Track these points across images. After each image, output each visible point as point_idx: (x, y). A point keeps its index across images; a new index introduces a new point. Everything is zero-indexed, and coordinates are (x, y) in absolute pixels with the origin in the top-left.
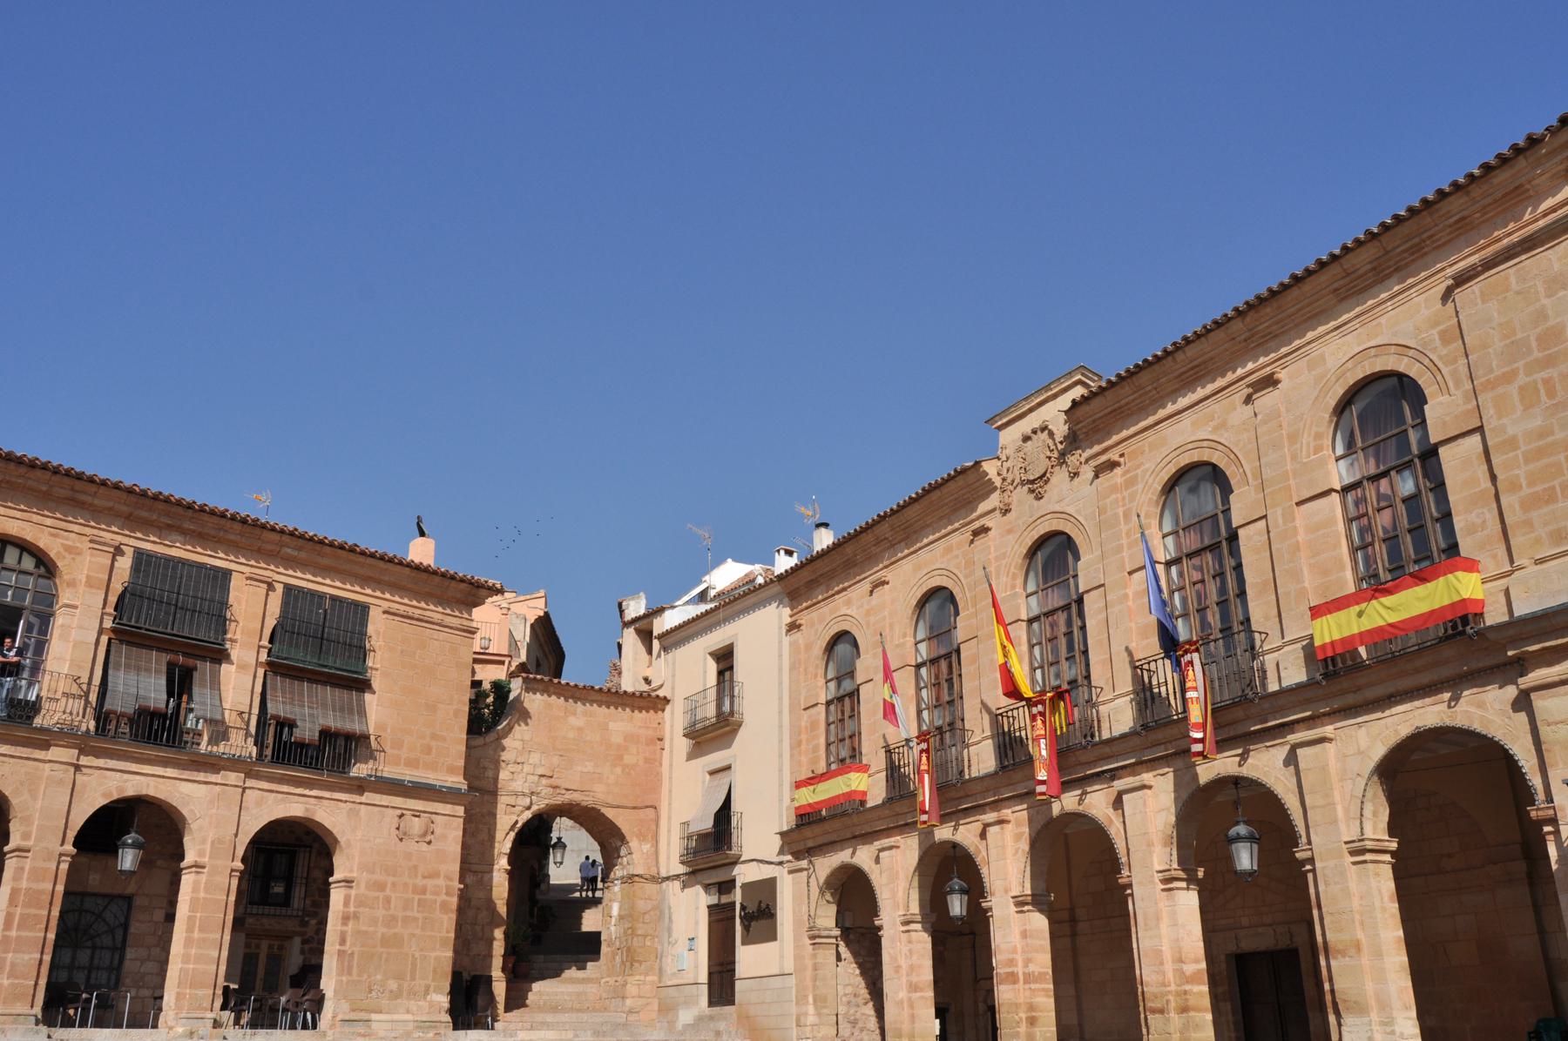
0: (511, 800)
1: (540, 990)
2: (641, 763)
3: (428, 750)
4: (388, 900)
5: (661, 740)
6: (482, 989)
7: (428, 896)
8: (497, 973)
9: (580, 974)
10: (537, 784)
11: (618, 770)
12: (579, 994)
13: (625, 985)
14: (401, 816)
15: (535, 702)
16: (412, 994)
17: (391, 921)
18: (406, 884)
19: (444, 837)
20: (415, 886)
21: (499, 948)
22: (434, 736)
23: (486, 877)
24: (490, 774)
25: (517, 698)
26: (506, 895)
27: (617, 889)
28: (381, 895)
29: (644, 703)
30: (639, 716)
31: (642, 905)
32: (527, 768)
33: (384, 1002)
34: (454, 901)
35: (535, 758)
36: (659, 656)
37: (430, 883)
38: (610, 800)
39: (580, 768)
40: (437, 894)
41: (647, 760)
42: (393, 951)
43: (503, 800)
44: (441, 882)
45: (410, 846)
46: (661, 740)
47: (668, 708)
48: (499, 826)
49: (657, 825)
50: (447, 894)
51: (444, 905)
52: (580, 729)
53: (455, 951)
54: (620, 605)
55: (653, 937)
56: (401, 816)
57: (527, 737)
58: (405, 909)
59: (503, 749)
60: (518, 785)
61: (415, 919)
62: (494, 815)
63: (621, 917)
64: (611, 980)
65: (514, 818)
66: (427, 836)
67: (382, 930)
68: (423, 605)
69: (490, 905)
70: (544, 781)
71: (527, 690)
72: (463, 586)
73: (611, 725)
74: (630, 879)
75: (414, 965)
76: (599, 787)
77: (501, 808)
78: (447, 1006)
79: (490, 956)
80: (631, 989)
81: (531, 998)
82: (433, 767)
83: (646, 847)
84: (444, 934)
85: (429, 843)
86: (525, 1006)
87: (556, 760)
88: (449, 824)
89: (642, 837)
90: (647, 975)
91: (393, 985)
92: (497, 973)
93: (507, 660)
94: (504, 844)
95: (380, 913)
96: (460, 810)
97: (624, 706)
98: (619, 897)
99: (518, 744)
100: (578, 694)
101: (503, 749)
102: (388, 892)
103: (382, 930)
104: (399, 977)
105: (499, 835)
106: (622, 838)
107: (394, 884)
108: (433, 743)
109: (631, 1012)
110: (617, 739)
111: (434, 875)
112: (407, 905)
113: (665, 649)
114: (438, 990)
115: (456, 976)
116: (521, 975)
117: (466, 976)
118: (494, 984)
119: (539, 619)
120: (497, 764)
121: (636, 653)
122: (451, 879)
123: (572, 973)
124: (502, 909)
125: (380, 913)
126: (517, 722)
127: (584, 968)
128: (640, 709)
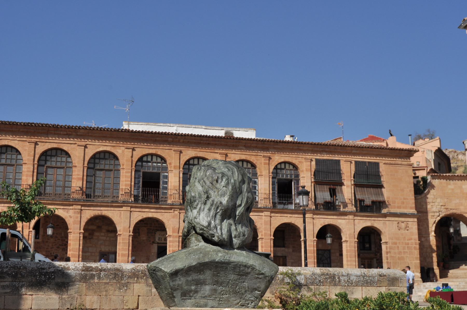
0: (433, 214)
3: (403, 203)
4: (398, 247)
6: (431, 272)
7: (410, 245)
10: (441, 208)
15: (436, 182)
17: (400, 253)
18: (403, 242)
19: (412, 228)
21: (435, 259)
22: (404, 199)
23: (428, 238)
24: (425, 207)
25: (430, 182)
28: (396, 246)
32: (436, 204)
34: (418, 246)
35: (439, 200)
37: (409, 241)
39: (454, 202)
43: (430, 215)
44: (413, 241)
45: (402, 231)
50: (415, 244)
51: (415, 248)
52: (453, 189)
56: (398, 223)
57: (435, 194)
60: (434, 209)
61: (407, 252)
65: (434, 220)
66: (407, 228)
69: (430, 246)
70: (443, 207)
71: (433, 179)
81: (449, 274)
82: (406, 208)
84: (416, 256)
87: (446, 200)
88: (413, 224)
93: (426, 168)
95: (397, 251)
96: (416, 220)
99: (432, 196)
102: (398, 245)
105: (430, 225)
108: (405, 201)
111: (411, 239)
112: (404, 248)
114: (417, 272)
117: (426, 268)
120: (426, 203)
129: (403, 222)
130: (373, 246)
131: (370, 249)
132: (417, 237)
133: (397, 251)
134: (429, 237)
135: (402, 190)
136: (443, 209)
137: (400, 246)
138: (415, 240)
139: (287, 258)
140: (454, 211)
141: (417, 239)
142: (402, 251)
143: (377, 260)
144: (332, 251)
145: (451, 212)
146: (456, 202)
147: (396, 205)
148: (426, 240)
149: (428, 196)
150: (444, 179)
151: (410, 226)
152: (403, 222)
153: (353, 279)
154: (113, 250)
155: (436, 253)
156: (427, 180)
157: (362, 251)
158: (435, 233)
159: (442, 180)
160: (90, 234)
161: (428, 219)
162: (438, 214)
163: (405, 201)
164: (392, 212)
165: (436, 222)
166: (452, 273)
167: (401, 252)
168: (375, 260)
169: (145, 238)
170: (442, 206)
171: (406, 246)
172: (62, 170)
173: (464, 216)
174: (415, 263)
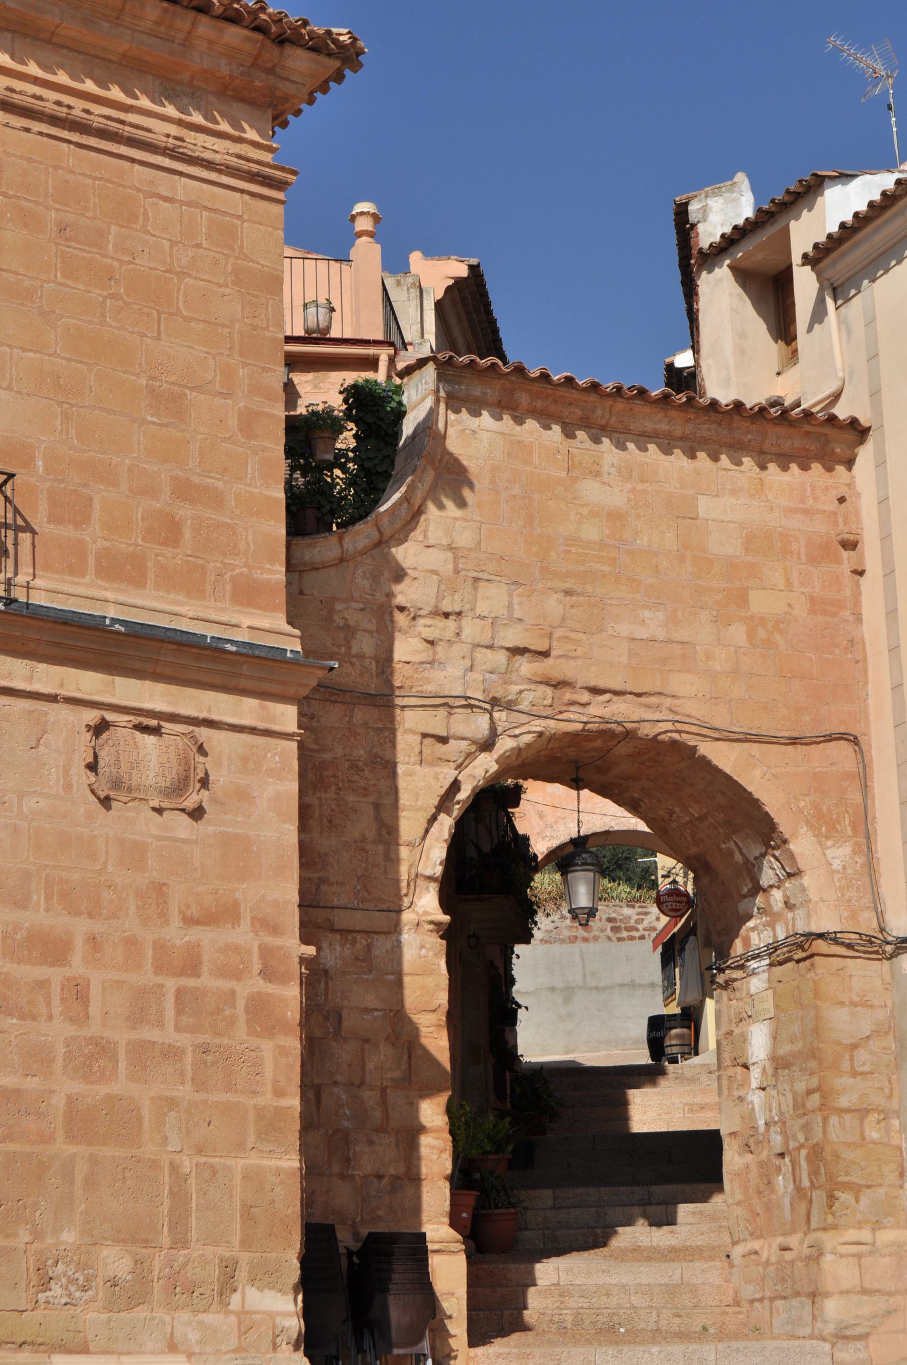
0: (435, 722)
1: (557, 1281)
2: (801, 611)
3: (169, 531)
4: (78, 992)
5: (850, 545)
6: (399, 1276)
7: (207, 981)
8: (437, 1229)
9: (661, 1237)
10: (507, 676)
11: (738, 634)
12: (672, 1291)
13: (816, 1255)
14: (100, 728)
15: (477, 437)
16: (182, 1290)
17: (94, 1057)
18: (131, 942)
19: (244, 796)
20: (161, 947)
21: (436, 1155)
22: (184, 491)
23: (381, 945)
24: (365, 644)
25: (427, 427)
26: (443, 998)
27: (756, 984)
28: (55, 975)
29: (792, 441)
30: (783, 480)
31: (842, 1023)
32: (471, 629)
33: (93, 1318)
34: (291, 995)
35: (492, 599)
36: (819, 314)
37: (208, 939)
38: (721, 719)
39: (625, 629)
40: (235, 973)
41: (817, 606)
42: (108, 1152)
43: (411, 722)
44: (243, 935)
45: (138, 822)
46: (850, 545)
47: (865, 454)
48: (404, 799)
49: (865, 788)
50: (267, 974)
51: (259, 1008)
52: (615, 517)
53: (305, 1150)
54: (682, 212)
55: (886, 1115)
56: (100, 728)
57: (464, 538)
58: (137, 1018)
59: (399, 575)
60: (450, 678)
61: (173, 1053)
62: (390, 768)
63: (779, 1063)
64: (768, 1248)
65: (448, 774)
66: (188, 795)
67: (66, 1086)
68: (116, 93)
69: (401, 1031)
70: (526, 667)
71: (454, 402)
72: (234, 34)
73: (704, 506)
74: (801, 948)
75: (179, 1197)
76: (689, 688)
77: (406, 744)
78: (294, 1325)
79: (415, 1179)
80: (837, 1270)
81: (537, 1303)
82: (190, 582)
83: (840, 854)
84: (267, 1099)
85: (197, 814)
86: (520, 1326)
87: (554, 606)
88: (257, 763)
89: (825, 826)
90: (877, 1226)
91: (116, 1262)
92: (437, 1229)
93: (384, 354)
94: (425, 852)
95: (57, 1032)
96: (286, 716)
97: (737, 449)
98: (768, 1005)
99: (438, 559)
100: (601, 412)
101: (399, 575)
102: (77, 966)
103: (66, 1086)
104: (136, 1236)
105: (409, 825)
106: (766, 832)
107: (93, 941)
108: (185, 511)
109: (842, 1336)
110: (725, 546)
111: (223, 914)
112: (141, 1009)
113: (838, 290)
114: (263, 1277)
115: (317, 1240)
116: (501, 1247)
117: (345, 1238)
118: (434, 1261)
119: (457, 288)
120: (384, 615)
121: (741, 335)
122: (276, 929)
123: (636, 1235)
124: (437, 1042)
125: (57, 1032)
126: (433, 495)
127: (671, 1221)
128: (784, 460)
129: (150, 724)
132: (287, 892)
134: (395, 929)
135: (172, 404)
136: (522, 681)
137: (96, 979)
138: (266, 924)
140: (622, 711)
141: (292, 918)
142: (122, 1037)
145: (602, 711)
146: (642, 633)
147: (94, 538)
148: (365, 960)
149: (405, 554)
150: (546, 419)
151: (219, 778)
152: (150, 724)
155: (443, 1099)
156: (400, 414)
158: (446, 904)
159: (531, 424)
161: (388, 768)
162: (480, 725)
163: (185, 511)
164: (39, 599)
165: (464, 794)
166: (561, 1291)
167: (102, 1049)
170: (517, 651)
171: (171, 984)
173: (706, 764)
174: (252, 1176)
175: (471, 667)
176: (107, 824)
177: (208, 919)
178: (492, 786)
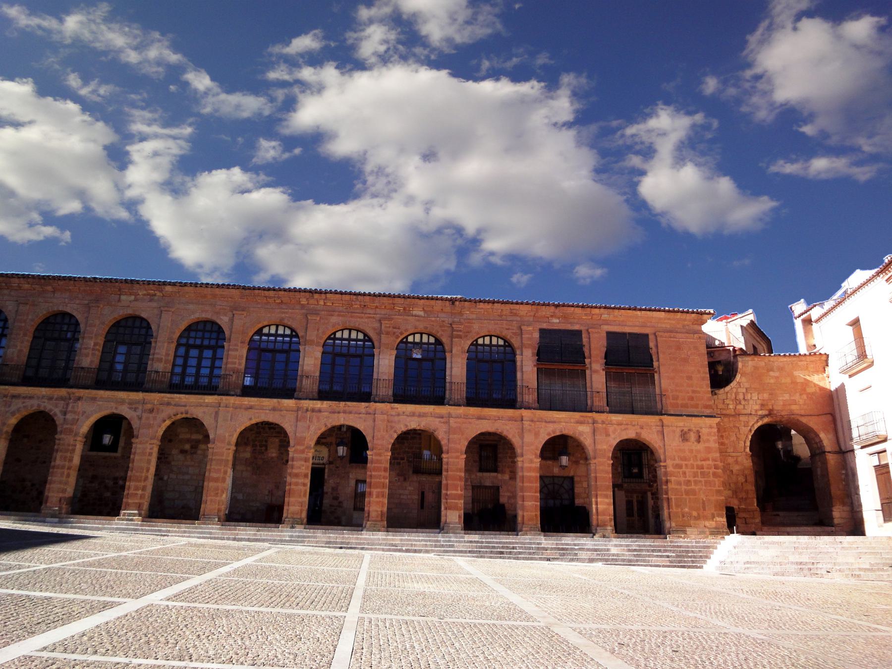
4: (684, 473)
17: (688, 483)
22: (694, 392)
28: (681, 471)
38: (803, 412)
52: (777, 378)
61: (700, 481)
67: (684, 487)
91: (695, 514)
102: (684, 469)
103: (684, 487)
111: (708, 459)
112: (695, 475)
114: (720, 516)
130: (645, 471)
131: (640, 475)
133: (682, 479)
137: (687, 471)
139: (501, 490)
142: (692, 479)
143: (652, 494)
144: (576, 479)
153: (158, 354)
154: (122, 474)
157: (626, 480)
160: (192, 447)
167: (689, 481)
168: (649, 494)
169: (274, 455)
172: (139, 347)
175: (862, 355)
176: (686, 446)
177: (704, 460)
178: (775, 425)
